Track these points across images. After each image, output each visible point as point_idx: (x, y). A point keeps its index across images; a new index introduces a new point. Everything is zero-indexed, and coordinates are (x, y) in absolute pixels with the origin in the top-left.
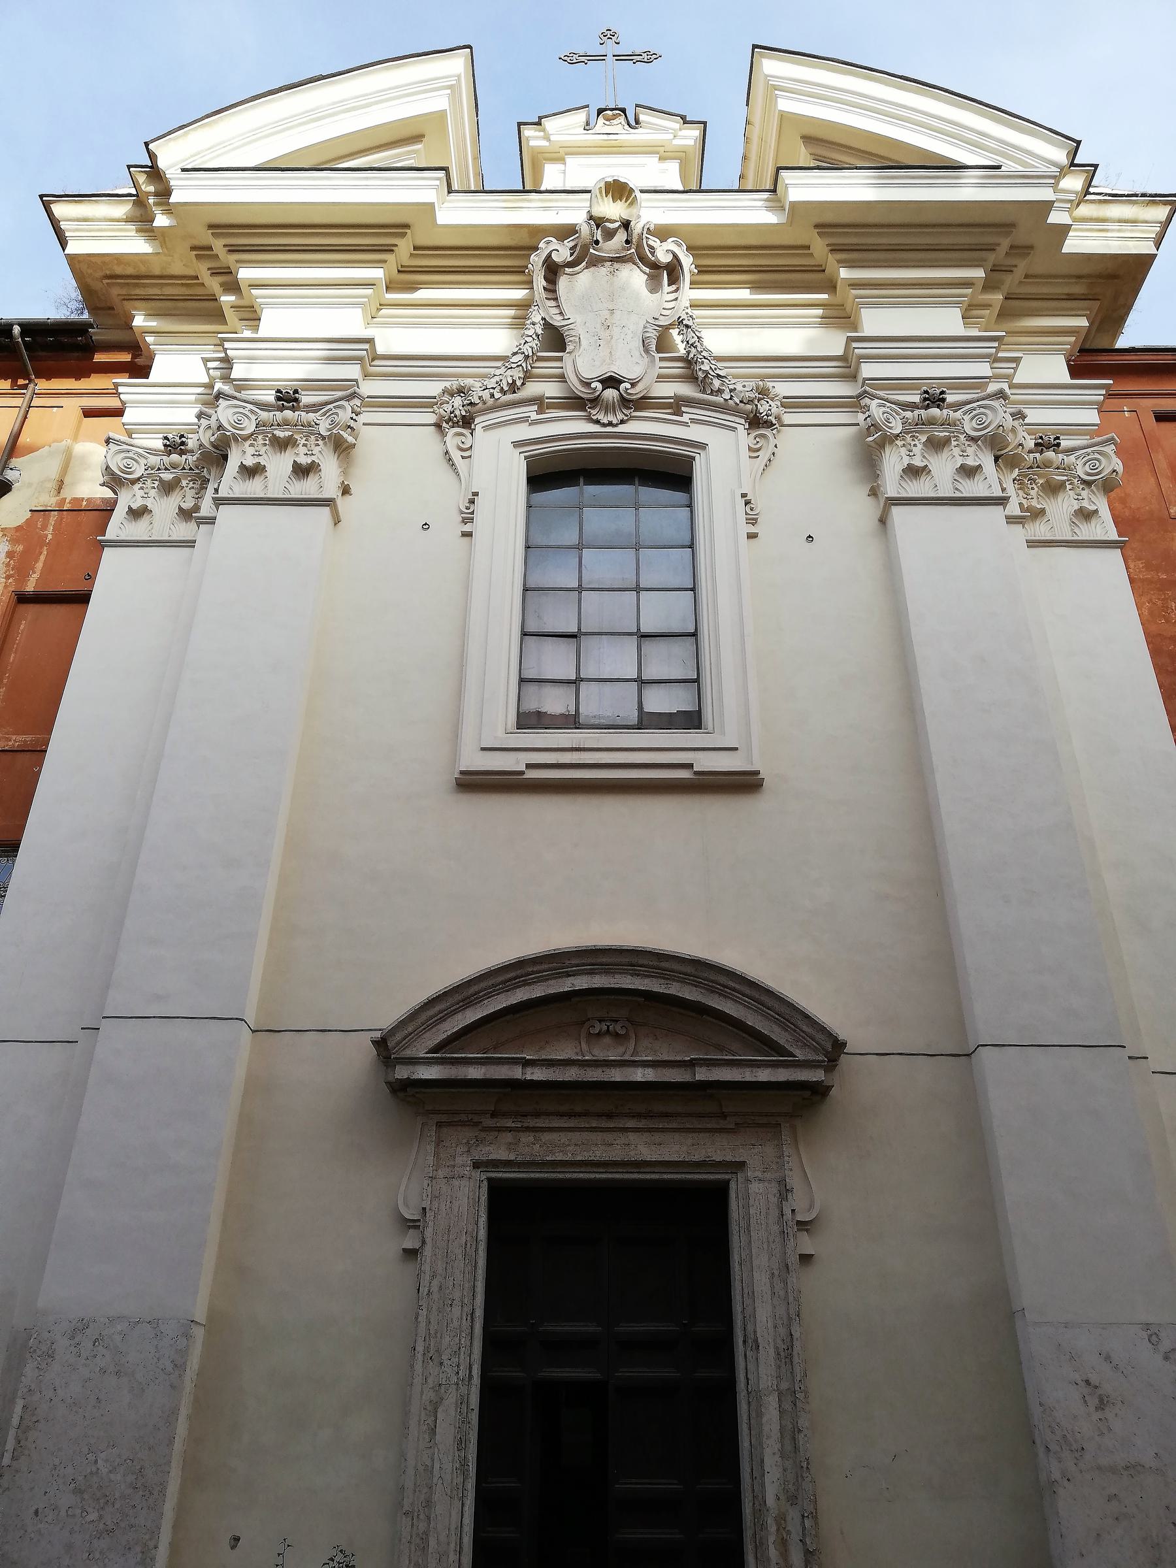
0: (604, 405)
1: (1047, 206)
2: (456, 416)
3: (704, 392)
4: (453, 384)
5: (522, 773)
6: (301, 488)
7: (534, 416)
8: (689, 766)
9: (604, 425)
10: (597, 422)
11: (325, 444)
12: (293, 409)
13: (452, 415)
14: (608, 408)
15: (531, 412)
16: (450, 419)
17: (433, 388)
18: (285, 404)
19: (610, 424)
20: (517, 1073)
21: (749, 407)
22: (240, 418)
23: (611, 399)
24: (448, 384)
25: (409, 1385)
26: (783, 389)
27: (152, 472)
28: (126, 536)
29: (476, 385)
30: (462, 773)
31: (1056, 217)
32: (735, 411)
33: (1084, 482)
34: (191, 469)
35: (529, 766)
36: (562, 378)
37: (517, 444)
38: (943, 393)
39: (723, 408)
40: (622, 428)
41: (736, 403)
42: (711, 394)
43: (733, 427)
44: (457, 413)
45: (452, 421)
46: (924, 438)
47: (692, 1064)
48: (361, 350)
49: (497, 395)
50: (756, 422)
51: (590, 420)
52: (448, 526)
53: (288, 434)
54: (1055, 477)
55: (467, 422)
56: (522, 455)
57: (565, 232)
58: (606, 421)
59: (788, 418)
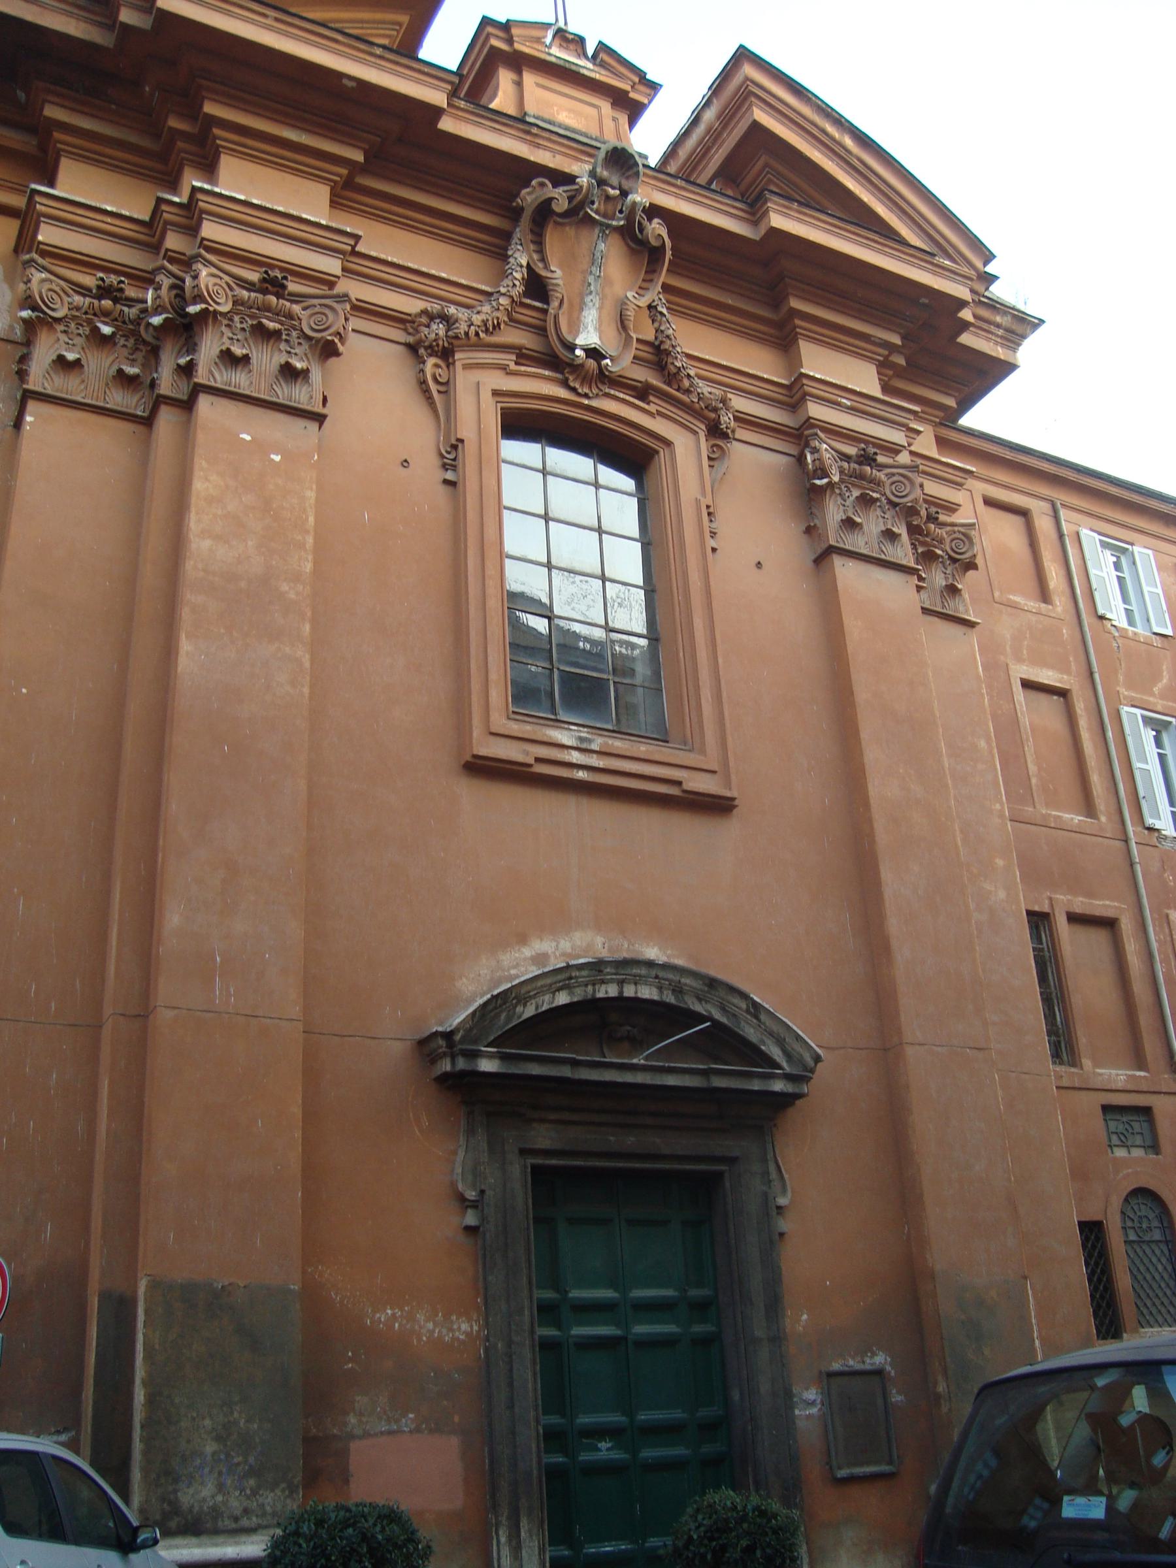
0: (583, 374)
1: (962, 304)
2: (438, 345)
3: (669, 384)
4: (434, 307)
5: (530, 766)
6: (286, 393)
7: (513, 366)
8: (679, 783)
9: (579, 394)
10: (574, 390)
11: (311, 347)
12: (279, 296)
13: (434, 344)
14: (586, 379)
15: (509, 359)
16: (430, 347)
17: (411, 305)
18: (270, 287)
19: (586, 396)
20: (566, 1072)
21: (713, 415)
22: (219, 292)
23: (591, 372)
24: (428, 306)
25: (1170, 1241)
26: (740, 403)
27: (77, 314)
28: (57, 391)
29: (462, 314)
30: (475, 756)
31: (966, 314)
32: (698, 414)
33: (890, 502)
34: (124, 322)
35: (538, 760)
36: (541, 331)
37: (496, 393)
38: (875, 454)
39: (688, 408)
40: (595, 403)
41: (702, 408)
42: (678, 390)
43: (695, 431)
44: (441, 343)
45: (432, 350)
46: (856, 493)
47: (705, 1073)
48: (345, 245)
49: (482, 335)
50: (716, 431)
51: (565, 384)
52: (427, 470)
53: (277, 326)
54: (871, 493)
55: (446, 355)
56: (499, 405)
57: (562, 178)
58: (572, 384)
59: (742, 434)
